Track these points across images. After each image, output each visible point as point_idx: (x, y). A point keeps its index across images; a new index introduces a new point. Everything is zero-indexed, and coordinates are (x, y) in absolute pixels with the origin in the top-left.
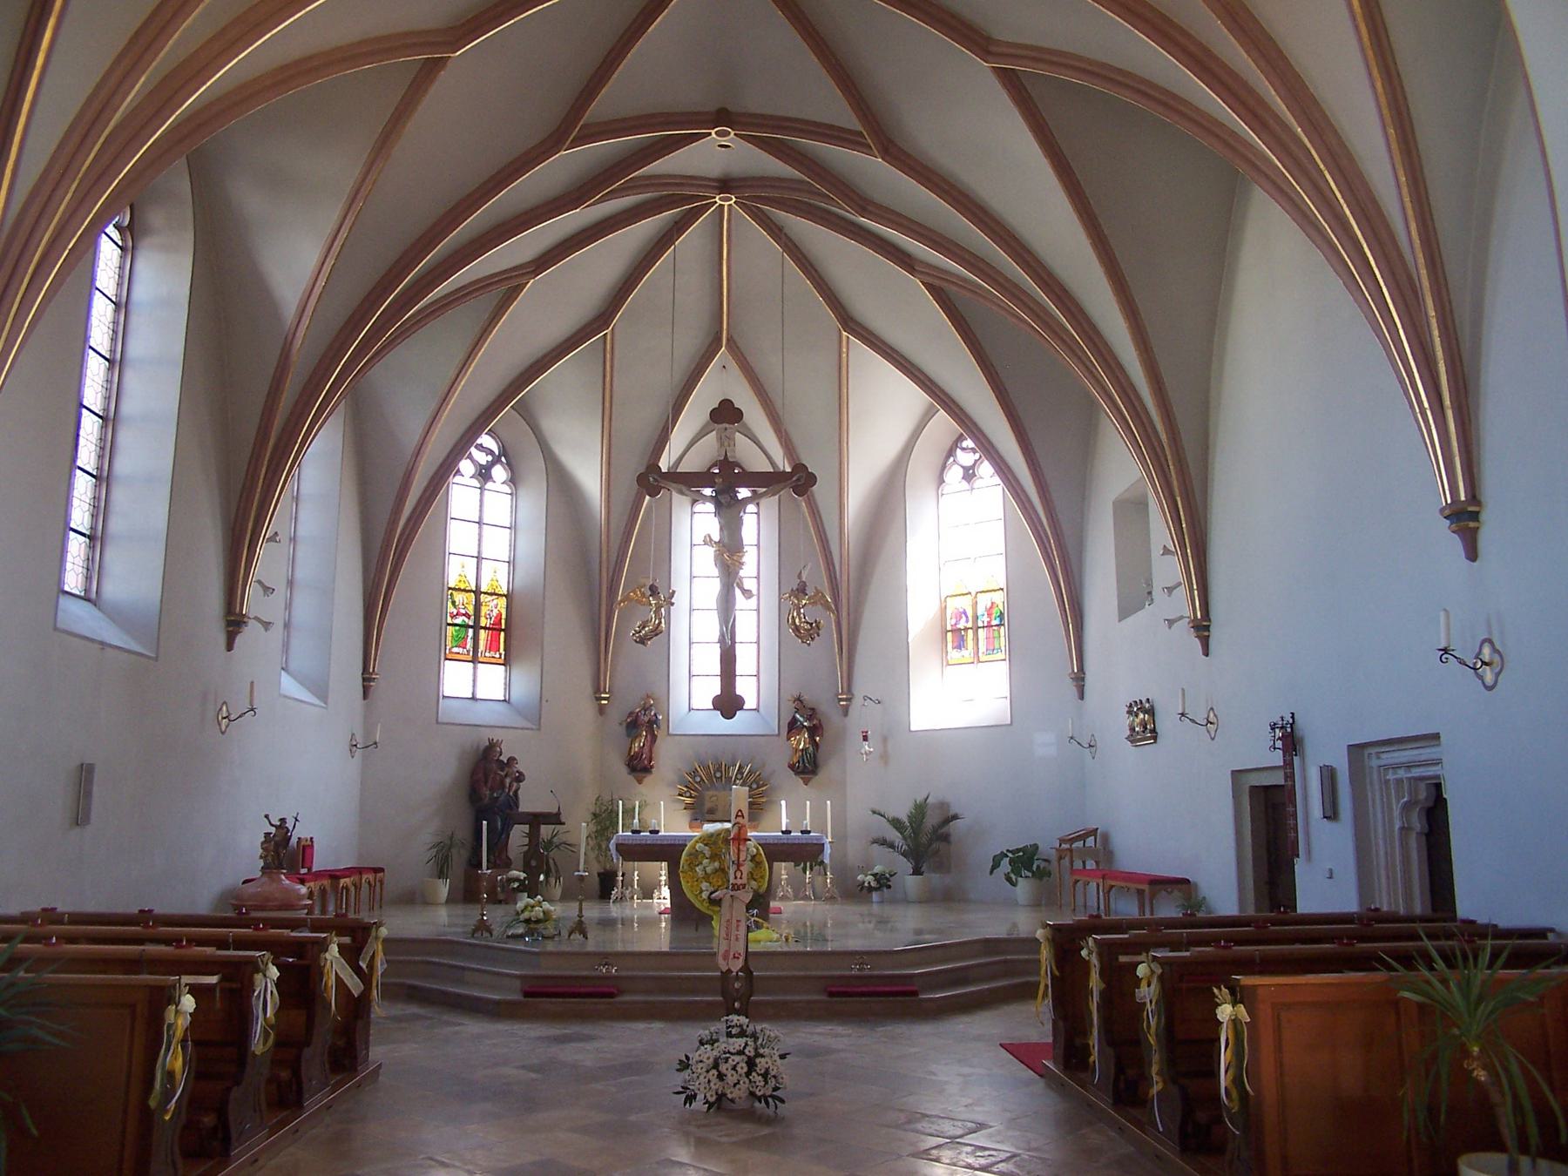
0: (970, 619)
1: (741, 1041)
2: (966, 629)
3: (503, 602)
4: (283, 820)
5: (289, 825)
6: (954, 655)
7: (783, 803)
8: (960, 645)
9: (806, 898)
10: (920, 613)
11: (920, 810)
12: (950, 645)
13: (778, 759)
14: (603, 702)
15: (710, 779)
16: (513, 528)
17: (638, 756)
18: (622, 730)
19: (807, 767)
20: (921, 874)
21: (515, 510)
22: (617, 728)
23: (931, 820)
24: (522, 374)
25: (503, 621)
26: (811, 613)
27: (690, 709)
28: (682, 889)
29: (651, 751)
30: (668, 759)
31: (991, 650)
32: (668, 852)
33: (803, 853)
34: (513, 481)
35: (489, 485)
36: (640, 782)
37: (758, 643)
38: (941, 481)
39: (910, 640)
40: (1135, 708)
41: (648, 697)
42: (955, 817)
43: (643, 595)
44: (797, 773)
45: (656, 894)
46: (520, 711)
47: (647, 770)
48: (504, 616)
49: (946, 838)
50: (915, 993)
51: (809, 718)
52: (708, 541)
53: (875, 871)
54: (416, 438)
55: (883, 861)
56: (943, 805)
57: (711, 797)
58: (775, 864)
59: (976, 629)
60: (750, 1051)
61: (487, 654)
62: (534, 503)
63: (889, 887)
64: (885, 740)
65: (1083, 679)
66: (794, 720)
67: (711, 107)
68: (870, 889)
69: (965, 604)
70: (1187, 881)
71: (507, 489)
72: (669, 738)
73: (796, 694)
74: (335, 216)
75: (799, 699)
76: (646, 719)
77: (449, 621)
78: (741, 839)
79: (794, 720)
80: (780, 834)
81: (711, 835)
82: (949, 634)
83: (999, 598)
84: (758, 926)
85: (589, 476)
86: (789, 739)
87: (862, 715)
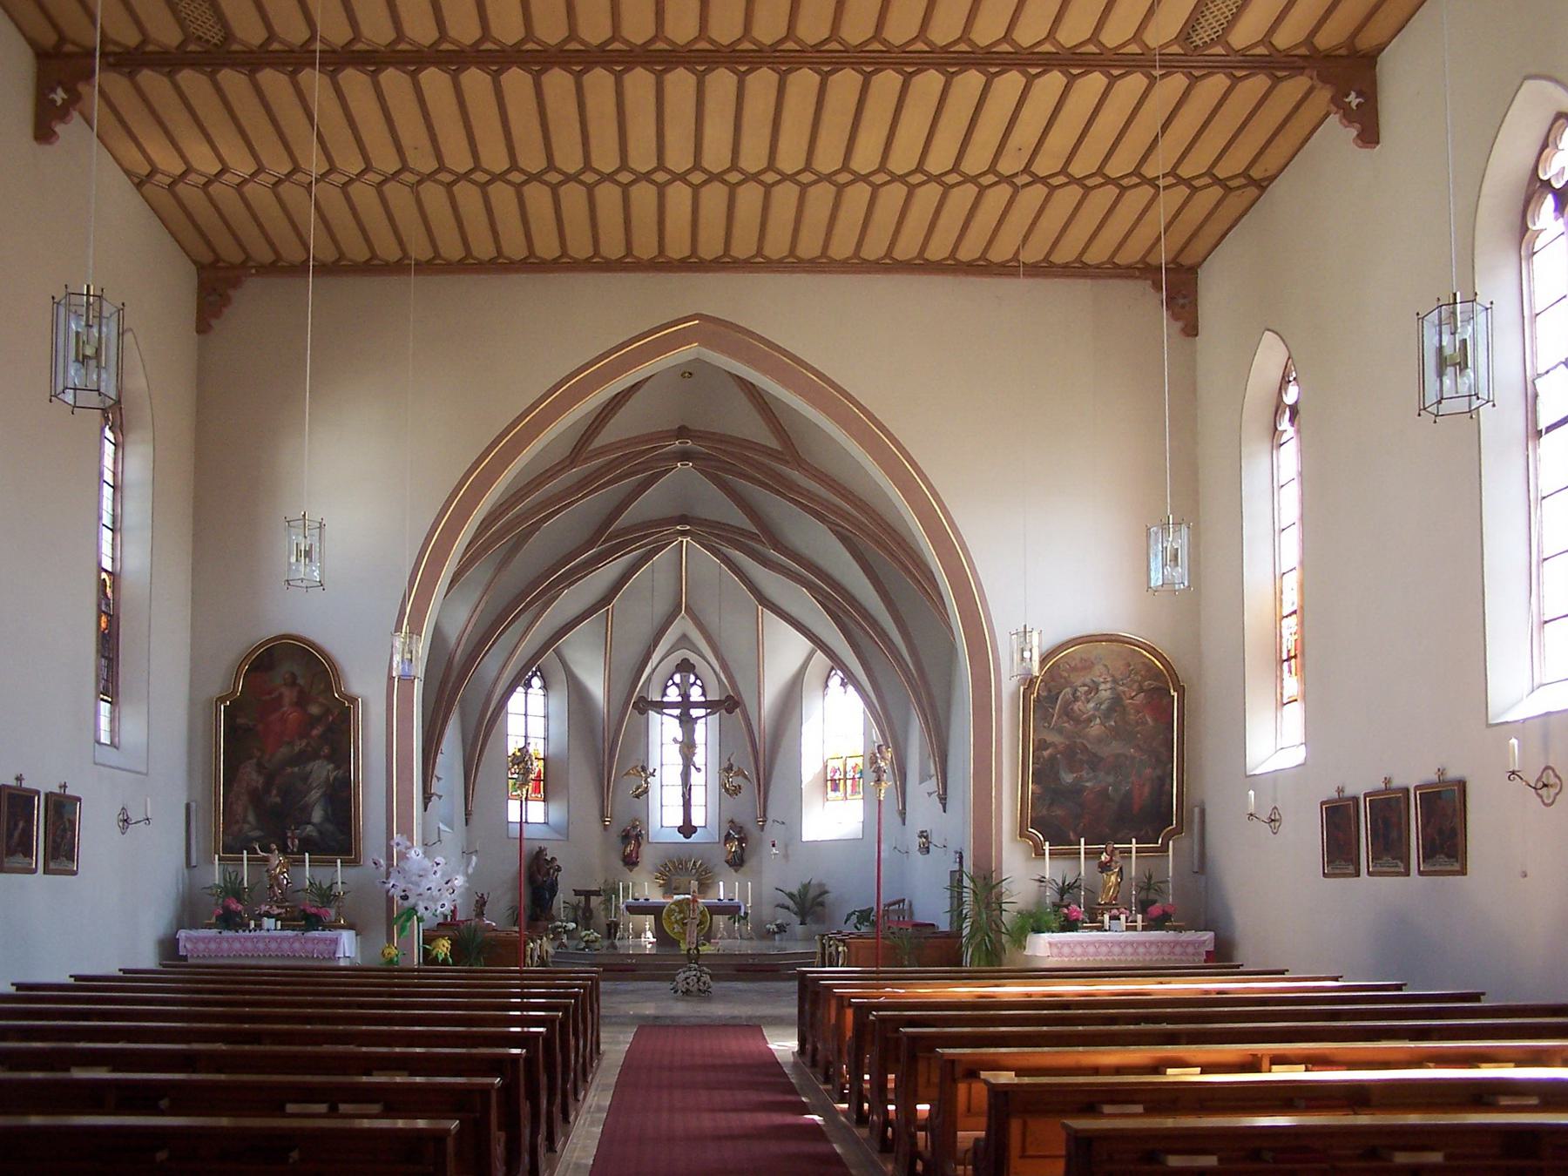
0: (842, 773)
1: (695, 972)
2: (839, 779)
3: (541, 763)
4: (482, 895)
5: (485, 897)
6: (831, 794)
7: (721, 883)
8: (835, 788)
9: (735, 938)
10: (810, 770)
11: (806, 887)
12: (829, 789)
13: (720, 854)
14: (607, 823)
15: (675, 868)
16: (546, 717)
17: (630, 854)
18: (619, 840)
19: (737, 862)
20: (805, 924)
21: (546, 706)
22: (615, 839)
23: (812, 893)
24: (557, 633)
25: (542, 775)
26: (737, 781)
27: (662, 826)
28: (665, 931)
29: (637, 853)
30: (647, 856)
31: (854, 792)
32: (655, 910)
33: (731, 910)
34: (545, 687)
35: (530, 690)
36: (631, 871)
37: (706, 806)
38: (826, 686)
39: (803, 786)
40: (922, 834)
41: (636, 820)
42: (826, 892)
43: (638, 771)
44: (730, 866)
45: (643, 935)
46: (556, 829)
47: (635, 864)
48: (542, 771)
49: (822, 904)
50: (778, 971)
51: (739, 833)
52: (675, 740)
53: (778, 923)
54: (494, 674)
55: (783, 917)
56: (821, 885)
57: (679, 880)
58: (714, 916)
59: (845, 779)
60: (699, 974)
61: (533, 795)
62: (559, 702)
63: (785, 931)
64: (786, 846)
65: (905, 813)
66: (729, 834)
67: (677, 513)
68: (774, 933)
69: (839, 764)
70: (933, 925)
71: (541, 692)
72: (649, 845)
73: (730, 819)
74: (478, 594)
75: (732, 821)
76: (635, 833)
77: (510, 776)
78: (695, 901)
79: (729, 834)
80: (717, 901)
81: (679, 901)
82: (829, 783)
83: (860, 761)
84: (704, 945)
85: (596, 686)
86: (725, 845)
87: (773, 831)
